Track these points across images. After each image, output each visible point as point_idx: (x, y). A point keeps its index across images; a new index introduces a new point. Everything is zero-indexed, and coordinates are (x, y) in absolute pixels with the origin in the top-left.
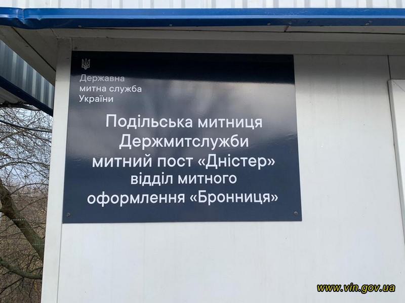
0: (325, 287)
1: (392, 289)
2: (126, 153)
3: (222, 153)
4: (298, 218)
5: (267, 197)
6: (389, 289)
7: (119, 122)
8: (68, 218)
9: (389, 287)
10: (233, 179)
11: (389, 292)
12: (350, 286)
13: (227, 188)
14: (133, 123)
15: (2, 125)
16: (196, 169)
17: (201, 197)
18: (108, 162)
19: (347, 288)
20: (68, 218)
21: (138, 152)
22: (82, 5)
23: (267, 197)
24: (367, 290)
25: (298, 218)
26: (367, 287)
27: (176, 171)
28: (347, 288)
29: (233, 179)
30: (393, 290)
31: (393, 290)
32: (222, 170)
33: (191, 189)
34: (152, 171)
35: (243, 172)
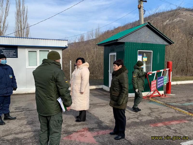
0: (155, 137)
1: (187, 138)
2: (4, 53)
3: (12, 53)
4: (18, 58)
5: (15, 56)
6: (185, 138)
7: (3, 51)
8: (115, 55)
9: (186, 137)
10: (13, 55)
11: (185, 140)
12: (167, 137)
13: (12, 56)
14: (4, 51)
15: (189, 101)
16: (10, 54)
17: (10, 56)
18: (2, 54)
19: (165, 138)
20: (115, 55)
21: (5, 53)
22: (172, 91)
23: (15, 56)
24: (175, 139)
25: (18, 58)
26: (175, 137)
27: (8, 54)
28: (165, 138)
29: (13, 55)
30: (187, 139)
31: (187, 139)
32: (12, 54)
33: (9, 56)
34: (6, 54)
35: (13, 55)
